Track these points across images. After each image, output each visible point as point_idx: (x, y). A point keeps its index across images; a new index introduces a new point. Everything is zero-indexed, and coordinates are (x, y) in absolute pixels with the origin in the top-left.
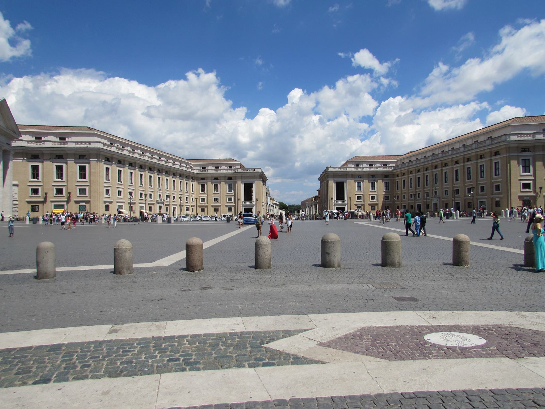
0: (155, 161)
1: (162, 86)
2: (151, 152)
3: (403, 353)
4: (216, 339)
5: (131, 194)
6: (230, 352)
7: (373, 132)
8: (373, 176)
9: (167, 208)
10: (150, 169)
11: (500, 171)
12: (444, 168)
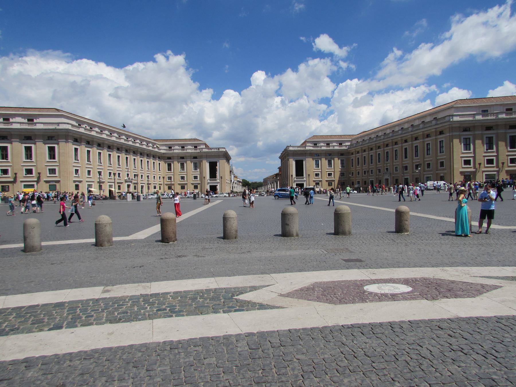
0: (122, 141)
1: (130, 68)
2: (118, 133)
3: (346, 299)
4: (195, 294)
5: (100, 173)
6: (207, 303)
7: (332, 112)
8: (330, 155)
9: (135, 187)
10: (118, 149)
12: (404, 145)
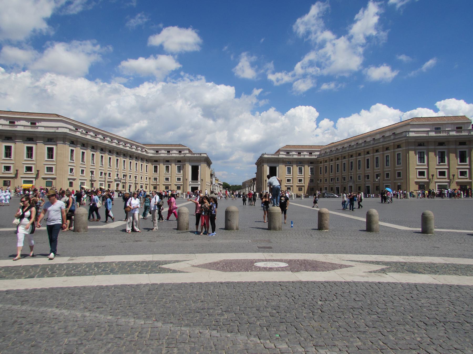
0: (114, 145)
5: (92, 172)
12: (366, 156)
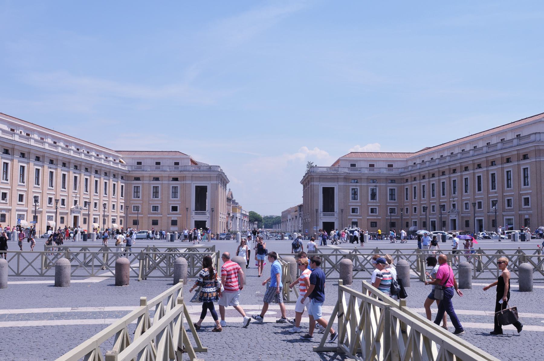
11: (529, 180)
12: (431, 179)
